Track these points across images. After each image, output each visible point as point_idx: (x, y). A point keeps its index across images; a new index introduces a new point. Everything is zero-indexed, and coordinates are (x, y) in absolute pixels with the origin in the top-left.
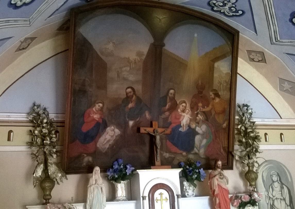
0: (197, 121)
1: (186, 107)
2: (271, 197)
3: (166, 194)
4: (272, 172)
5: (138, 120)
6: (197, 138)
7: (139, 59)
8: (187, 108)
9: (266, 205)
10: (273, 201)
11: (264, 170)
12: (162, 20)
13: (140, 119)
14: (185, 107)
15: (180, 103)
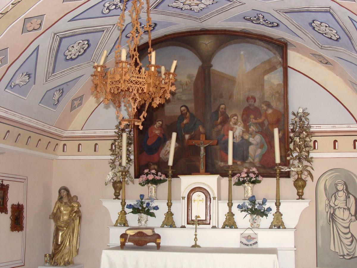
0: (249, 132)
1: (237, 120)
2: (333, 205)
3: (202, 196)
4: (337, 181)
5: (193, 133)
6: (251, 149)
7: (190, 81)
8: (239, 121)
9: (325, 213)
10: (335, 210)
11: (328, 179)
12: (208, 44)
13: (194, 132)
14: (236, 120)
15: (232, 117)
